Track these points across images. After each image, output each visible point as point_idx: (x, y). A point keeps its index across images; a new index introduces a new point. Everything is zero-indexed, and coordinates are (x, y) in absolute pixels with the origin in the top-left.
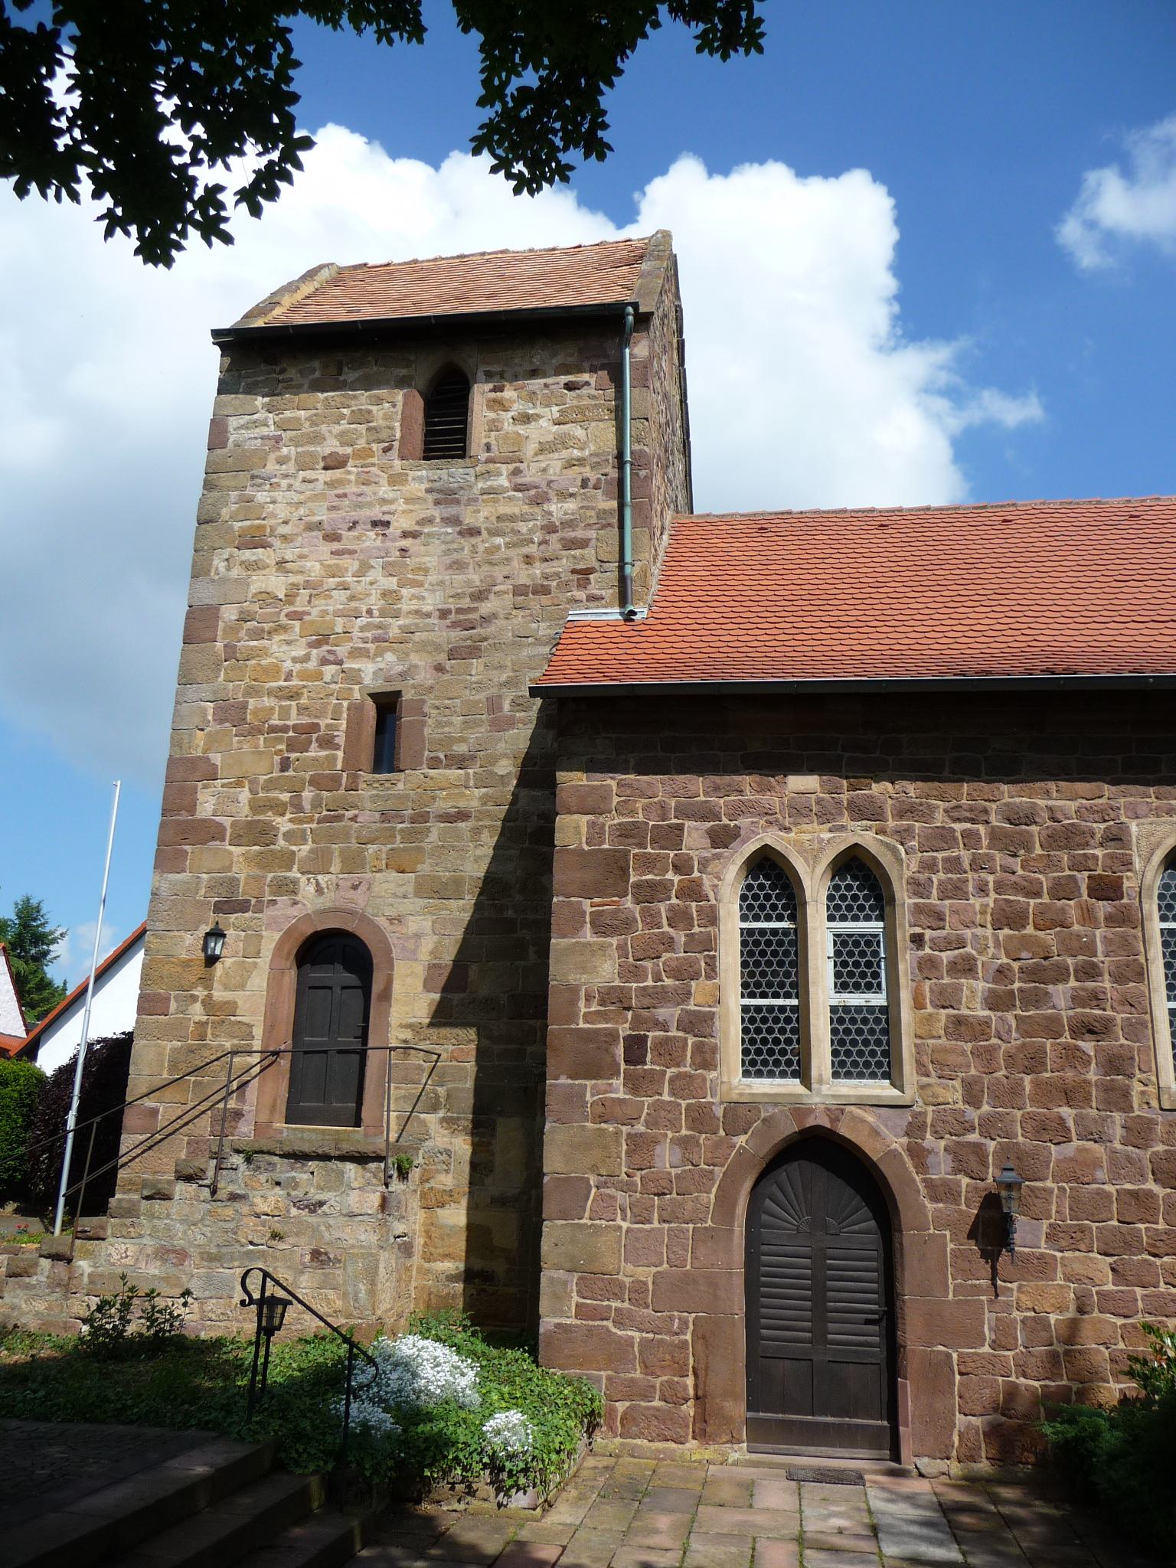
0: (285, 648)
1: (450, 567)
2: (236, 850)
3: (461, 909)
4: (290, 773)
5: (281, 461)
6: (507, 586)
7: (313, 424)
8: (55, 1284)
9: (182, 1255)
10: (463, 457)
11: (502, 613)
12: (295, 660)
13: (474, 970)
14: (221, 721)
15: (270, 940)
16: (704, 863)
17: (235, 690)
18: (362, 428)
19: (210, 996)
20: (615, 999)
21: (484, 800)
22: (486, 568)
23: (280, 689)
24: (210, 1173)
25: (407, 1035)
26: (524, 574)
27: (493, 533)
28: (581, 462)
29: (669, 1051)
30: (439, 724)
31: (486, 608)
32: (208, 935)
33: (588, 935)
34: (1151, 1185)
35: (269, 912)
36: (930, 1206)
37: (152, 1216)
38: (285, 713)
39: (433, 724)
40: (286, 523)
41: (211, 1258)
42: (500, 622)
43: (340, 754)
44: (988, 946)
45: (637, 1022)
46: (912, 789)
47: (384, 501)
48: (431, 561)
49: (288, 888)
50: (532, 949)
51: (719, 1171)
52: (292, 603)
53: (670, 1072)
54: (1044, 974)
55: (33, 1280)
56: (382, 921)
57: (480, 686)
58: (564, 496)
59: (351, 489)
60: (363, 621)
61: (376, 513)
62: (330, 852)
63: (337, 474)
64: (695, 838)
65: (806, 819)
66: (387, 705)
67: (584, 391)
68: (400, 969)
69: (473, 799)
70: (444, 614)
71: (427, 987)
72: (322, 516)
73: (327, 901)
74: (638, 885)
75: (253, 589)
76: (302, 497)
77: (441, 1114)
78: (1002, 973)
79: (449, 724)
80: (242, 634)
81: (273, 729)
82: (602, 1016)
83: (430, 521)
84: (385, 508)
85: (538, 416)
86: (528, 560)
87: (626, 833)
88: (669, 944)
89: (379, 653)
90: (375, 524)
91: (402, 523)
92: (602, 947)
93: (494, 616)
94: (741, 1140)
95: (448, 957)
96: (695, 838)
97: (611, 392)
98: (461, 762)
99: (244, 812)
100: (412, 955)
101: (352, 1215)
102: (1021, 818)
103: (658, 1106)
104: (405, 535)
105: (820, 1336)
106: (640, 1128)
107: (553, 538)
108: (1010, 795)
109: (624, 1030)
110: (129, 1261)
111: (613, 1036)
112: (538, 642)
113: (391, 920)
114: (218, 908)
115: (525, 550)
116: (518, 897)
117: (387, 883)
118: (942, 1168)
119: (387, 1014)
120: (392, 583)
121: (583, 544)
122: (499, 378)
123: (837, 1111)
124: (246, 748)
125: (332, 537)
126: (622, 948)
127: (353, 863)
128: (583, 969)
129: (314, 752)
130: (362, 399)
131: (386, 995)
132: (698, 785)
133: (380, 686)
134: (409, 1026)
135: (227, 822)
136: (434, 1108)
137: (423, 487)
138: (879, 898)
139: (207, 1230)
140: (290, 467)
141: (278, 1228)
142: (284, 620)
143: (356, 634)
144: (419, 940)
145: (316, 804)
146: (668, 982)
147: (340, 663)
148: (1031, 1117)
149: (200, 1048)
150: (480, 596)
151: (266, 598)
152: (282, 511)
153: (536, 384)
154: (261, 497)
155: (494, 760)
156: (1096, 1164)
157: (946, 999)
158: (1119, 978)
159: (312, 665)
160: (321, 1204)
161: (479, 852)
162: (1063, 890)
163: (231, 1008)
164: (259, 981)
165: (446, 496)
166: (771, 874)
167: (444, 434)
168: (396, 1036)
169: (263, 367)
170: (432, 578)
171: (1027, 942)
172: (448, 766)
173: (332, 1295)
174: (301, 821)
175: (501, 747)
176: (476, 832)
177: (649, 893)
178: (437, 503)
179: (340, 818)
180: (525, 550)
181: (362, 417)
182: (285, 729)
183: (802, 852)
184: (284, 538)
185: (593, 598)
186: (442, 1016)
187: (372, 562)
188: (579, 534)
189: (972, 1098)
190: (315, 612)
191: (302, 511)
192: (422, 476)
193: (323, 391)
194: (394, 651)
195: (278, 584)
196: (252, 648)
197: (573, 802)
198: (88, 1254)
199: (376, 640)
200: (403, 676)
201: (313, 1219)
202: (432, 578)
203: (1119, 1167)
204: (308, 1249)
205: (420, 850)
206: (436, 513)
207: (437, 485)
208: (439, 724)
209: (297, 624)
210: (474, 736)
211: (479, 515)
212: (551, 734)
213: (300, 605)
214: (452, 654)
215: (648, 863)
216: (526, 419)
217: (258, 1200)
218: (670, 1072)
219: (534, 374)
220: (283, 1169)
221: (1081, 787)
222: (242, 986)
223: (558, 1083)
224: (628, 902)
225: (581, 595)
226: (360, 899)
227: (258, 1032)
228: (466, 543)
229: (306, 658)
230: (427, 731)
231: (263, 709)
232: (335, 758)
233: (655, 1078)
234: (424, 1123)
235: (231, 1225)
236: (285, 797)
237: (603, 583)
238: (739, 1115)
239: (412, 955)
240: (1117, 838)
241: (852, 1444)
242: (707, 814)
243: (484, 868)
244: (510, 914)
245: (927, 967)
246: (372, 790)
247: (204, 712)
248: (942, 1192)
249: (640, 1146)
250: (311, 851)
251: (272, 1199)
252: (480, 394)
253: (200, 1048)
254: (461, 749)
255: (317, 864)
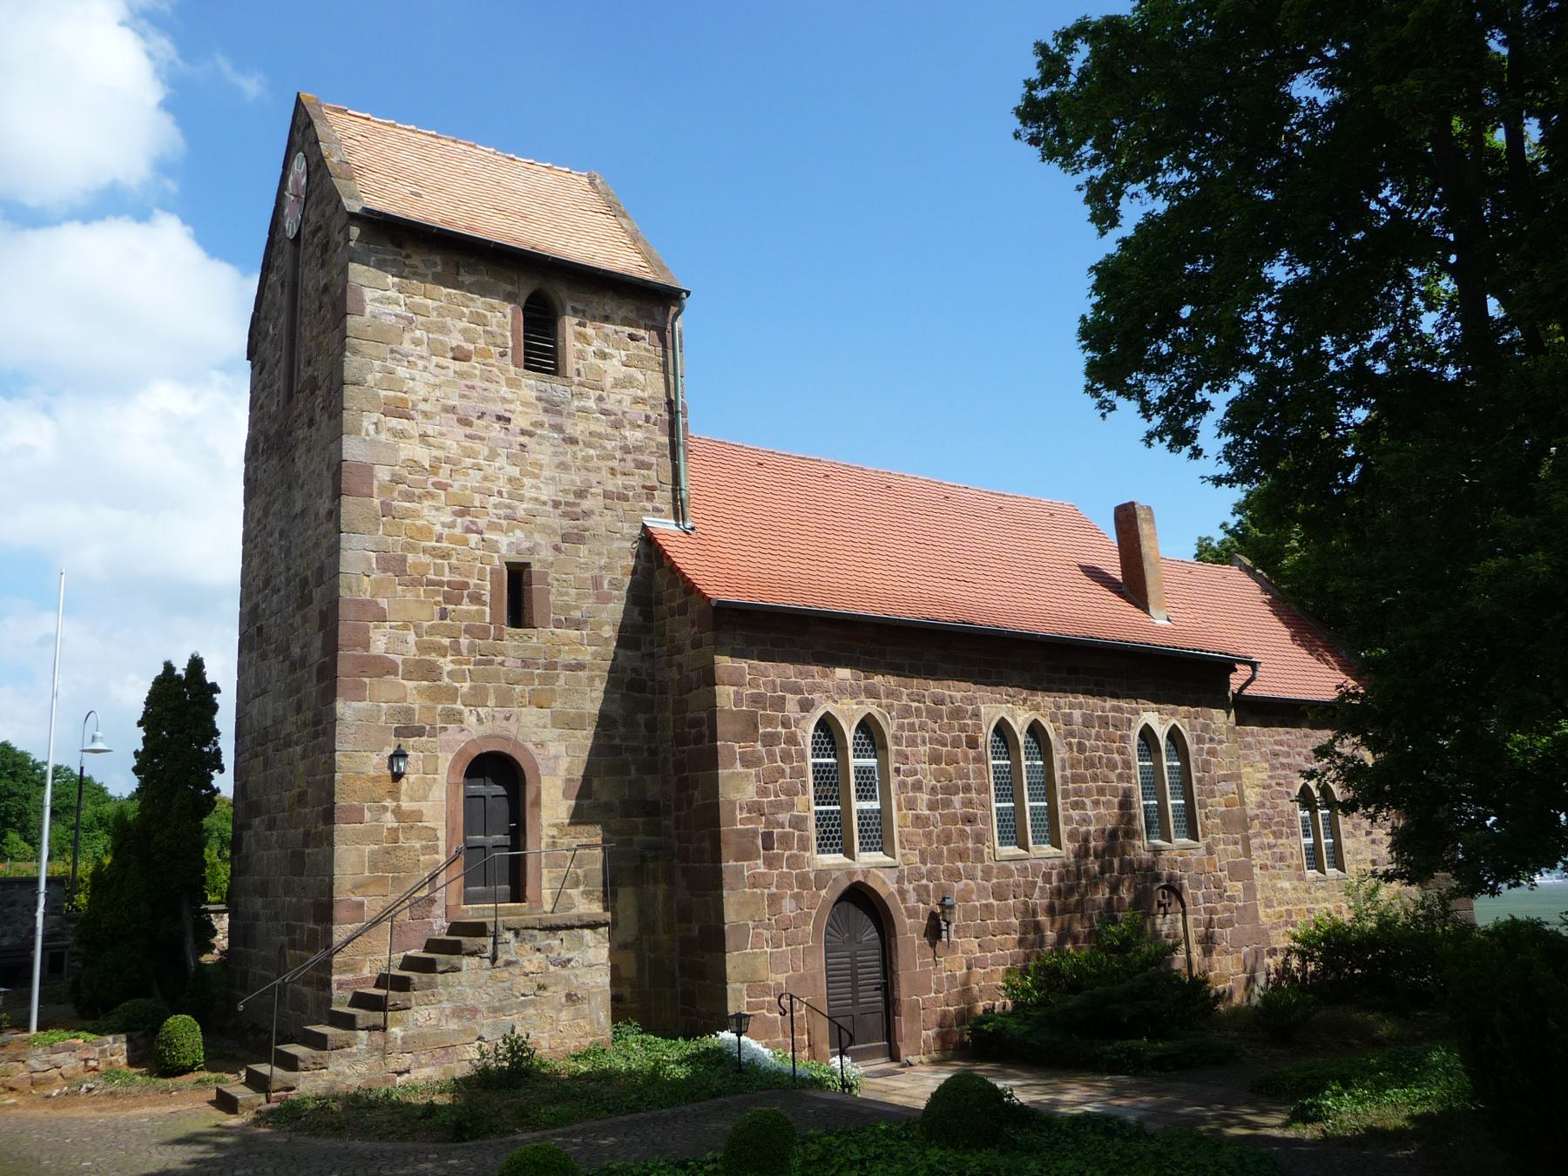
0: (434, 513)
1: (558, 467)
2: (410, 684)
3: (585, 737)
4: (448, 621)
5: (417, 342)
6: (598, 490)
7: (440, 315)
8: (373, 1049)
9: (474, 1011)
10: (555, 373)
11: (597, 511)
12: (444, 525)
13: (596, 783)
14: (385, 570)
15: (445, 761)
16: (797, 722)
17: (394, 544)
18: (480, 328)
19: (399, 807)
20: (756, 809)
21: (595, 655)
22: (583, 472)
23: (434, 548)
24: (490, 948)
25: (554, 832)
26: (610, 482)
27: (588, 445)
28: (643, 401)
29: (786, 840)
30: (560, 594)
31: (586, 504)
32: (392, 757)
33: (739, 768)
34: (992, 901)
35: (443, 736)
36: (908, 921)
37: (446, 985)
38: (439, 570)
39: (557, 590)
40: (425, 400)
41: (495, 1010)
42: (596, 518)
43: (487, 609)
44: (927, 773)
45: (768, 824)
46: (892, 680)
47: (504, 400)
48: (545, 459)
49: (454, 717)
50: (633, 768)
51: (814, 912)
52: (436, 474)
53: (787, 853)
54: (950, 790)
55: (354, 1050)
56: (530, 746)
57: (585, 567)
58: (635, 426)
59: (477, 383)
60: (495, 499)
61: (499, 408)
62: (485, 689)
63: (464, 366)
64: (792, 707)
65: (843, 693)
66: (518, 577)
67: (641, 344)
68: (546, 782)
69: (587, 654)
70: (556, 504)
71: (566, 796)
72: (454, 401)
73: (487, 729)
74: (764, 735)
75: (403, 455)
76: (437, 381)
77: (581, 888)
78: (933, 789)
79: (567, 594)
80: (396, 494)
81: (431, 583)
82: (750, 820)
83: (542, 425)
84: (507, 406)
85: (612, 356)
86: (613, 471)
87: (757, 700)
88: (782, 772)
89: (510, 530)
90: (499, 418)
91: (519, 422)
92: (747, 775)
93: (592, 512)
94: (823, 892)
95: (579, 773)
96: (792, 707)
97: (660, 349)
98: (577, 625)
99: (412, 652)
100: (553, 772)
101: (591, 966)
102: (939, 701)
103: (781, 876)
104: (523, 433)
105: (856, 1002)
106: (774, 890)
107: (629, 457)
108: (935, 688)
109: (761, 829)
110: (433, 1022)
111: (755, 832)
112: (623, 538)
113: (536, 745)
114: (399, 733)
115: (610, 464)
116: (622, 730)
117: (531, 715)
118: (912, 898)
119: (539, 817)
120: (515, 471)
121: (648, 466)
122: (584, 315)
123: (866, 873)
124: (409, 596)
125: (464, 422)
126: (757, 775)
127: (504, 700)
128: (738, 790)
129: (466, 606)
130: (479, 303)
131: (537, 802)
132: (790, 669)
133: (515, 558)
134: (555, 825)
135: (399, 659)
136: (576, 885)
137: (534, 394)
138: (831, 737)
139: (490, 991)
140: (423, 350)
141: (542, 981)
142: (431, 489)
143: (491, 510)
144: (557, 762)
145: (472, 649)
146: (783, 797)
147: (481, 533)
148: (946, 868)
149: (395, 849)
150: (581, 494)
151: (413, 465)
152: (422, 391)
153: (609, 328)
154: (402, 371)
155: (600, 625)
156: (972, 892)
157: (911, 804)
158: (979, 792)
159: (458, 531)
160: (569, 960)
161: (594, 695)
162: (956, 743)
163: (417, 816)
164: (439, 793)
165: (552, 407)
166: (827, 726)
167: (540, 351)
168: (547, 832)
169: (390, 247)
170: (546, 473)
171: (943, 772)
172: (568, 627)
173: (582, 1022)
174: (461, 663)
175: (604, 615)
176: (591, 679)
177: (770, 740)
178: (546, 411)
179: (491, 662)
180: (610, 464)
181: (479, 319)
182: (440, 583)
183: (844, 717)
184: (425, 414)
185: (657, 510)
186: (579, 817)
187: (499, 451)
188: (645, 458)
189: (924, 862)
190: (456, 485)
191: (438, 393)
192: (531, 384)
193: (446, 286)
194: (522, 529)
195: (423, 455)
196: (407, 509)
197: (726, 678)
198: (398, 1022)
199: (507, 517)
200: (531, 550)
201: (564, 972)
202: (546, 473)
203: (982, 891)
204: (563, 994)
205: (553, 691)
206: (545, 418)
207: (544, 395)
208: (560, 594)
209: (442, 493)
210: (587, 604)
211: (577, 428)
212: (637, 610)
213: (443, 477)
214: (565, 538)
215: (769, 721)
216: (603, 356)
217: (526, 964)
218: (787, 853)
219: (606, 319)
220: (542, 939)
221: (963, 684)
222: (425, 798)
223: (729, 864)
224: (759, 745)
225: (649, 506)
226: (512, 728)
227: (442, 834)
228: (570, 448)
229: (452, 525)
230: (552, 598)
231: (422, 564)
232: (484, 613)
233: (779, 857)
234: (570, 896)
235: (507, 984)
236: (446, 641)
237: (663, 498)
238: (822, 876)
239: (553, 772)
240: (976, 715)
241: (874, 1057)
242: (797, 690)
243: (598, 705)
244: (617, 741)
245: (902, 785)
246: (513, 640)
247: (368, 560)
248: (913, 913)
249: (774, 900)
250: (471, 688)
251: (535, 962)
252: (569, 325)
253: (395, 849)
254: (576, 614)
255: (477, 698)
